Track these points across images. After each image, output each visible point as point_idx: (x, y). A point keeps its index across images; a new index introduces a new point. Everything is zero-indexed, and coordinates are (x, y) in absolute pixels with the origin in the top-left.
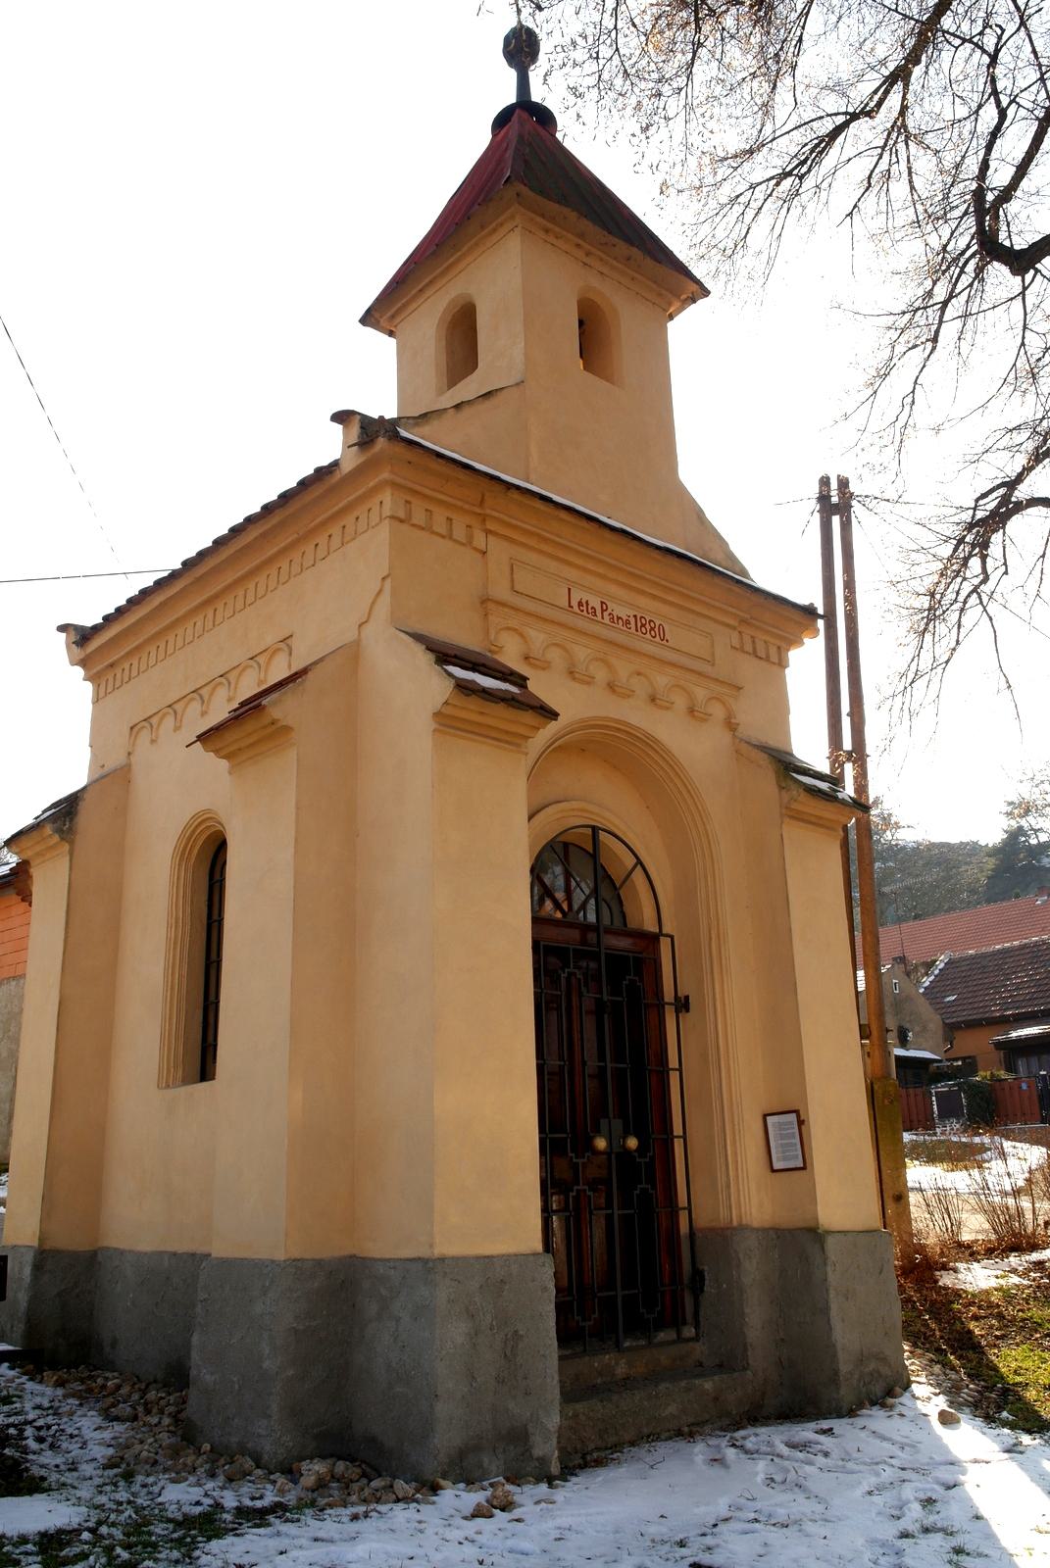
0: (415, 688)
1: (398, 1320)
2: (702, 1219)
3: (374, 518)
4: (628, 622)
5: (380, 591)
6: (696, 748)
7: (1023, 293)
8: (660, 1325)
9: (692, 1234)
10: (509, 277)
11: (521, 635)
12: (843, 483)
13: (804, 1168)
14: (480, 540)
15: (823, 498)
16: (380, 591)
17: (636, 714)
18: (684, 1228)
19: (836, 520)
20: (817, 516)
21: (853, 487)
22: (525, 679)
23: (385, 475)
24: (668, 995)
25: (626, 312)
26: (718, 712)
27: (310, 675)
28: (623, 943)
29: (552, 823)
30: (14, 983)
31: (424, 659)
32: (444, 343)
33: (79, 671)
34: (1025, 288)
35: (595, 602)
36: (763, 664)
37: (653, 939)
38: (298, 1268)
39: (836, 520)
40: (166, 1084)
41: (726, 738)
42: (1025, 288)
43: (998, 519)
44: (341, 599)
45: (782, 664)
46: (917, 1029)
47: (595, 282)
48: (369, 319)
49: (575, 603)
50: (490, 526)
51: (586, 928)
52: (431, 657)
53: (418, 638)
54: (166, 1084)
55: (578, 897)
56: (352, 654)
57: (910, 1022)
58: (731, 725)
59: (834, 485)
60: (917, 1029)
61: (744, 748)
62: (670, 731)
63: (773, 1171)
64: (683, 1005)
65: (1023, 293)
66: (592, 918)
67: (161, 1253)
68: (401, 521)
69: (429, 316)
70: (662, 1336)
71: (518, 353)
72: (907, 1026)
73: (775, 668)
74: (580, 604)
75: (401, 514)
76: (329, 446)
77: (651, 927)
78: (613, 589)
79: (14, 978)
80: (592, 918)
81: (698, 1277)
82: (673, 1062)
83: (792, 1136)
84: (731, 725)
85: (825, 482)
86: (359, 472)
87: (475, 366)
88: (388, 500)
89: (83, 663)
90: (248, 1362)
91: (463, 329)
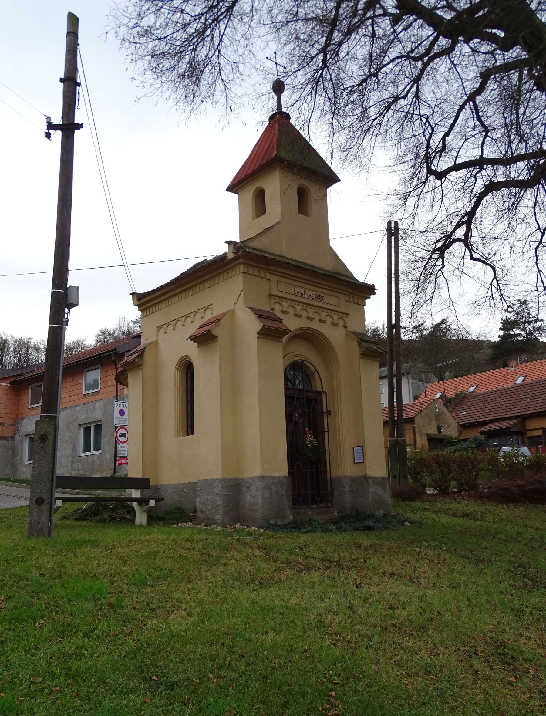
0: (250, 325)
1: (252, 491)
2: (333, 476)
3: (238, 273)
4: (313, 296)
5: (240, 295)
6: (334, 335)
7: (441, 185)
8: (321, 502)
9: (331, 478)
10: (274, 185)
11: (280, 304)
12: (396, 223)
13: (363, 462)
14: (268, 276)
15: (389, 229)
16: (240, 295)
17: (315, 326)
18: (329, 477)
19: (393, 238)
20: (386, 236)
21: (400, 226)
22: (282, 320)
23: (241, 260)
24: (325, 410)
25: (313, 190)
26: (341, 323)
27: (222, 320)
28: (311, 394)
29: (289, 361)
30: (70, 409)
31: (253, 316)
32: (254, 202)
33: (137, 307)
34: (442, 184)
35: (302, 291)
36: (357, 305)
37: (320, 393)
38: (223, 480)
39: (393, 238)
40: (177, 436)
41: (343, 331)
42: (442, 184)
43: (446, 246)
44: (231, 298)
45: (364, 305)
46: (446, 426)
47: (302, 182)
48: (229, 189)
49: (296, 292)
50: (271, 272)
51: (300, 390)
52: (256, 316)
53: (251, 308)
54: (177, 436)
55: (297, 382)
56: (232, 313)
57: (443, 423)
58: (345, 327)
59: (393, 225)
60: (446, 426)
61: (350, 334)
62: (326, 330)
63: (355, 463)
64: (329, 413)
65: (441, 185)
66: (301, 387)
67: (180, 484)
68: (245, 273)
69: (249, 193)
70: (322, 505)
71: (278, 211)
72: (442, 425)
73: (361, 306)
74: (298, 292)
75: (246, 272)
76: (223, 249)
77: (319, 389)
78: (308, 286)
79: (70, 407)
80: (301, 387)
81: (333, 490)
82: (326, 429)
83: (360, 453)
84: (345, 327)
85: (389, 223)
86: (233, 260)
87: (264, 212)
88: (242, 268)
89: (139, 306)
90: (211, 503)
91: (260, 197)
